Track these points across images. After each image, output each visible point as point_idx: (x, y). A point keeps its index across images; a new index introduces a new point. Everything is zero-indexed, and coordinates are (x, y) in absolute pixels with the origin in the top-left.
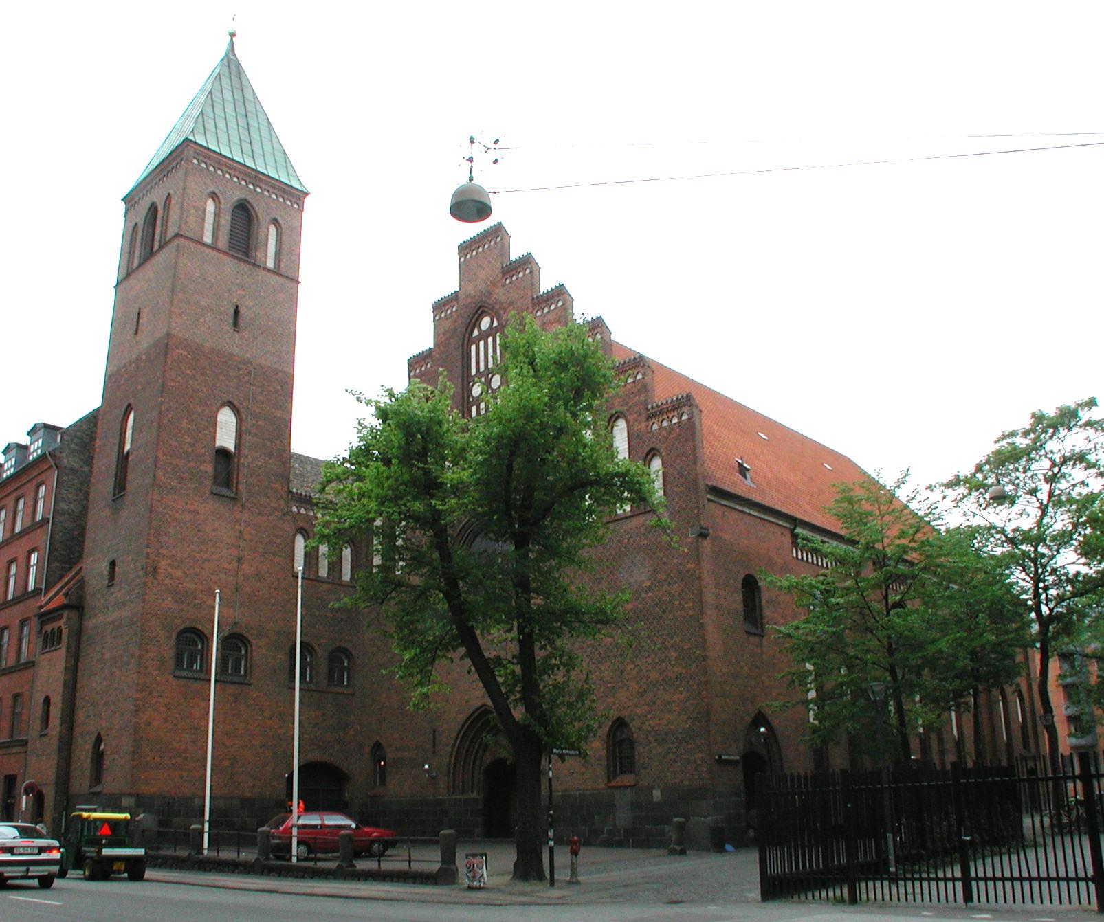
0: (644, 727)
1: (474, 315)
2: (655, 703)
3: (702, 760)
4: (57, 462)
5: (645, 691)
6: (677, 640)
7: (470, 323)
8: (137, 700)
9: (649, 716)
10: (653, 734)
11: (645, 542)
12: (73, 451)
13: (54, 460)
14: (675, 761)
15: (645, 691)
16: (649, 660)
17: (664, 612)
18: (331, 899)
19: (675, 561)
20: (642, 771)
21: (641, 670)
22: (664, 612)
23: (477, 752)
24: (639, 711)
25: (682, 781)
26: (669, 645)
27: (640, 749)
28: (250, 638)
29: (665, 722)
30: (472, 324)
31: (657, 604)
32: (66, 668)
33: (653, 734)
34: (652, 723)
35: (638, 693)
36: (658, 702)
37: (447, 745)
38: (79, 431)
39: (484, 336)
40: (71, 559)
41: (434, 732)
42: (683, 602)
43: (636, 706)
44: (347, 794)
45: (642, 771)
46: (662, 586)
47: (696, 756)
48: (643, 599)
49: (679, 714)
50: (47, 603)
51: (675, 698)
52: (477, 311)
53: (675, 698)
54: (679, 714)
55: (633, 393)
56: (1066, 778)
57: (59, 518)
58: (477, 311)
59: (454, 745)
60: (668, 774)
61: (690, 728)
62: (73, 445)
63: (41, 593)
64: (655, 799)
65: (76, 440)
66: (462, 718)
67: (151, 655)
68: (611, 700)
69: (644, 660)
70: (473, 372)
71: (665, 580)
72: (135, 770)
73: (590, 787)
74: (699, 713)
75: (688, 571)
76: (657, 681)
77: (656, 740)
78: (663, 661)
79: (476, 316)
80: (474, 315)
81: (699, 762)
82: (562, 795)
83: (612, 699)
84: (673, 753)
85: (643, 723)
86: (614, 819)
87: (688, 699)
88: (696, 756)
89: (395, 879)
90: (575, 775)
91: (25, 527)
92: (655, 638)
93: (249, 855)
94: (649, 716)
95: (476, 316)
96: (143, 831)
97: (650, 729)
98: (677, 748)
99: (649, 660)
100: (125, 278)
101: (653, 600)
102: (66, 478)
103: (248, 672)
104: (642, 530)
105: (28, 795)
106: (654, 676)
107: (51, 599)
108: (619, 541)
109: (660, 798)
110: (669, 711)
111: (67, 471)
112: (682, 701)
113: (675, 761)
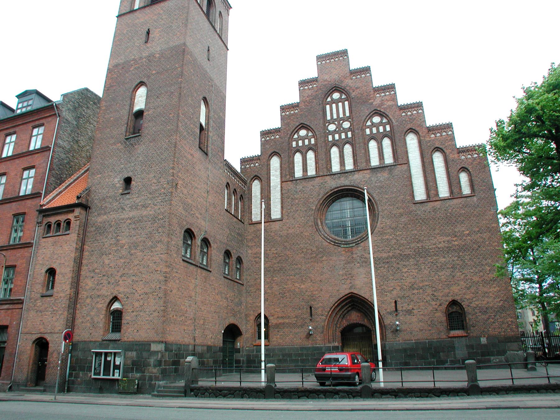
0: (471, 305)
1: (330, 90)
2: (477, 293)
3: (512, 322)
4: (59, 112)
5: (470, 287)
6: (490, 261)
7: (327, 94)
8: (166, 272)
9: (474, 299)
10: (478, 308)
11: (463, 212)
12: (69, 109)
13: (58, 111)
14: (494, 323)
15: (470, 287)
16: (472, 271)
17: (479, 247)
18: (328, 409)
19: (484, 222)
20: (472, 328)
21: (466, 276)
22: (479, 247)
23: (338, 320)
24: (468, 297)
25: (500, 332)
26: (484, 263)
27: (469, 317)
28: (211, 242)
29: (485, 302)
30: (328, 94)
31: (474, 243)
32: (76, 249)
33: (478, 308)
34: (476, 303)
35: (466, 287)
36: (480, 292)
37: (322, 315)
38: (74, 98)
39: (334, 101)
40: (61, 178)
41: (311, 308)
42: (491, 243)
43: (464, 294)
44: (238, 344)
45: (472, 328)
46: (477, 234)
47: (508, 320)
48: (465, 240)
49: (494, 298)
50: (48, 203)
51: (491, 290)
52: (332, 89)
53: (491, 290)
54: (494, 298)
55: (447, 140)
56: (551, 337)
57: (57, 149)
58: (332, 89)
59: (327, 315)
60: (490, 329)
61: (502, 305)
62: (69, 105)
63: (41, 196)
64: (482, 343)
65: (71, 103)
66: (333, 300)
67: (173, 243)
68: (446, 291)
69: (468, 271)
70: (329, 118)
71: (478, 231)
72: (165, 324)
73: (436, 338)
74: (508, 298)
75: (493, 227)
76: (478, 282)
77: (480, 312)
78: (481, 271)
79: (331, 91)
80: (330, 90)
81: (510, 323)
82: (415, 343)
83: (448, 290)
84: (493, 318)
85: (471, 303)
86: (455, 354)
87: (500, 291)
88: (508, 320)
89: (322, 396)
90: (424, 331)
91: (43, 146)
92: (475, 260)
93: (311, 382)
94: (474, 299)
95: (331, 91)
96: (193, 369)
97: (475, 306)
98: (495, 316)
99: (472, 271)
100: (144, 7)
101: (471, 241)
102: (63, 124)
103: (209, 263)
104: (461, 206)
105: (65, 341)
106: (476, 279)
107: (51, 201)
108: (445, 210)
109: (486, 342)
110: (487, 297)
111: (64, 120)
112: (495, 292)
113: (494, 323)
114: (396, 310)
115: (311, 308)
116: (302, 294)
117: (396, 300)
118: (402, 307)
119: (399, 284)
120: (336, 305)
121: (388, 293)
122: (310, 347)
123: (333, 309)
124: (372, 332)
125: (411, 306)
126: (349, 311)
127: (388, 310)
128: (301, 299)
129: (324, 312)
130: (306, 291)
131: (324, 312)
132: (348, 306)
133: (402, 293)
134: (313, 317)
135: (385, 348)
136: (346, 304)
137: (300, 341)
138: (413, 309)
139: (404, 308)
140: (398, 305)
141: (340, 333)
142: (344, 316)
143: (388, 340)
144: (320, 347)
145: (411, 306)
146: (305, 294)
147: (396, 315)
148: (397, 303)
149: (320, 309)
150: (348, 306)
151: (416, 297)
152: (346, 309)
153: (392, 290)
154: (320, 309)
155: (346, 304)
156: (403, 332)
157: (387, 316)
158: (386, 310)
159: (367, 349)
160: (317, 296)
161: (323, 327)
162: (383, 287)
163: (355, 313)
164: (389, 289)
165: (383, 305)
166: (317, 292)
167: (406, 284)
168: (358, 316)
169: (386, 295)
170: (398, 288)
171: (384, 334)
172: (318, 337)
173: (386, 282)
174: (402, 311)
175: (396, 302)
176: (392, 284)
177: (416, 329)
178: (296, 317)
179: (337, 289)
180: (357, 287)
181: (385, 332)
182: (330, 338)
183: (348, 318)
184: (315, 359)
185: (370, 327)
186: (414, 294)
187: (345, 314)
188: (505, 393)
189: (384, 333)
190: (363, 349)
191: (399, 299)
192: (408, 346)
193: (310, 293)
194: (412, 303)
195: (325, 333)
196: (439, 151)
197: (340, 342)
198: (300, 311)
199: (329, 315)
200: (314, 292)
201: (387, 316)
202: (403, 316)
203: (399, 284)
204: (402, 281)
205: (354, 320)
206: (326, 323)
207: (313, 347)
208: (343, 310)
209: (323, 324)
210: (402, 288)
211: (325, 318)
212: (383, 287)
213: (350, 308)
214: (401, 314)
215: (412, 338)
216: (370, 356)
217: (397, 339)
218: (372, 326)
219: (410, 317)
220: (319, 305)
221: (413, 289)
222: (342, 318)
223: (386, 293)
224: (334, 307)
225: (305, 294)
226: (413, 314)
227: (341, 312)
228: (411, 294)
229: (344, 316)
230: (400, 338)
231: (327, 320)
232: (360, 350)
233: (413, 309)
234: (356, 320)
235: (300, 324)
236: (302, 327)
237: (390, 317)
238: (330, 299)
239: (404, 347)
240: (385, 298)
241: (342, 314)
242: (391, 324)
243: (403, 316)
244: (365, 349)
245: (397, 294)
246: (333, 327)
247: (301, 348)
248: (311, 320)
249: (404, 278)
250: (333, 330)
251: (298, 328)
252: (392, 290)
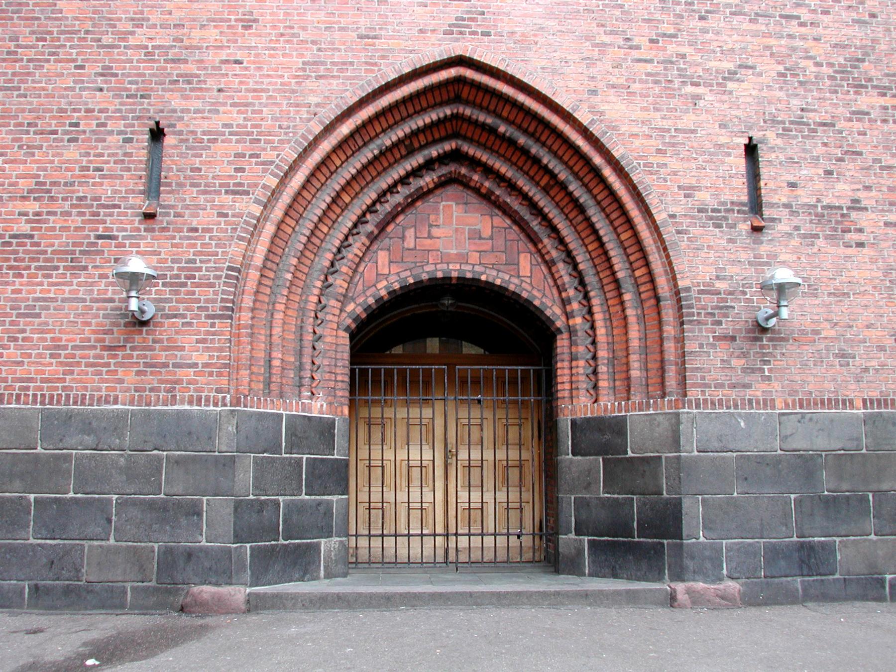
23: (344, 245)
37: (238, 191)
59: (275, 193)
114: (756, 204)
115: (157, 134)
116: (107, 40)
117: (756, 135)
118: (792, 185)
119: (772, 42)
120: (345, 129)
121: (700, 90)
122: (121, 416)
123: (316, 157)
124: (562, 343)
125: (842, 187)
126: (422, 195)
127: (704, 197)
128: (91, 70)
129: (252, 169)
130: (138, 22)
131: (252, 169)
132: (418, 159)
133: (795, 103)
134: (167, 199)
135: (675, 443)
136: (407, 147)
137: (53, 368)
138: (856, 205)
139: (805, 197)
140: (764, 171)
141: (344, 339)
142: (382, 227)
143: (694, 393)
144: (205, 414)
145: (842, 187)
146: (124, 36)
147: (756, 229)
148: (764, 155)
149: (224, 151)
150: (418, 159)
151: (874, 136)
152: (403, 180)
153: (731, 75)
154: (224, 151)
155: (407, 147)
156: (789, 347)
157: (695, 231)
158: (689, 191)
159: (489, 455)
160: (213, 57)
161: (237, 272)
162: (672, 49)
163: (456, 210)
164: (713, 64)
165: (673, 164)
166: (212, 34)
167: (819, 51)
168: (476, 235)
169: (697, 97)
170: (770, 68)
171: (671, 352)
172: (188, 340)
173: (696, 23)
174: (793, 213)
175: (751, 150)
176: (731, 41)
177: (873, 334)
178: (40, 191)
179: (364, 22)
180: (504, 27)
181: (680, 340)
182: (277, 354)
183: (410, 242)
184: (151, 506)
185: (553, 311)
186: (861, 114)
187: (392, 217)
188: (526, 601)
189: (670, 346)
190: (463, 455)
191: (771, 135)
192: (821, 443)
193: (163, 38)
194: (850, 168)
195: (245, 317)
196: (464, 183)
197: (343, 393)
198: (72, 153)
199: (286, 198)
200: (196, 34)
201: (695, 231)
202: (795, 242)
203: (772, 42)
204: (793, 28)
205: (446, 259)
206: (261, 250)
207: (148, 415)
208: (383, 183)
209: (236, 250)
210: (792, 71)
211: (243, 305)
212: (672, 49)
213: (428, 180)
214: (783, 227)
215: (852, 391)
216: (502, 496)
217: (758, 391)
218: (565, 302)
219: (842, 251)
220: (216, 123)
221: (859, 87)
222: (373, 238)
223: (689, 89)
224: (326, 146)
225: (124, 36)
226: (853, 237)
227: (370, 195)
228: (845, 112)
229: (382, 227)
230: (776, 386)
231: (269, 229)
232: (447, 454)
233: (856, 205)
234: (463, 258)
235: (61, 241)
236: (77, 268)
237: (717, 237)
238: (309, 84)
239: (799, 443)
240: (688, 121)
241: (371, 209)
242: (721, 285)
243: (795, 242)
244: (476, 455)
245: (760, 101)
246: (306, 288)
247: (48, 417)
248: (149, 216)
249: (805, 16)
250: (302, 310)
251: (48, 269)
252: (731, 75)
